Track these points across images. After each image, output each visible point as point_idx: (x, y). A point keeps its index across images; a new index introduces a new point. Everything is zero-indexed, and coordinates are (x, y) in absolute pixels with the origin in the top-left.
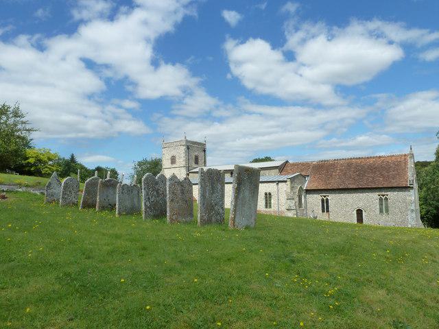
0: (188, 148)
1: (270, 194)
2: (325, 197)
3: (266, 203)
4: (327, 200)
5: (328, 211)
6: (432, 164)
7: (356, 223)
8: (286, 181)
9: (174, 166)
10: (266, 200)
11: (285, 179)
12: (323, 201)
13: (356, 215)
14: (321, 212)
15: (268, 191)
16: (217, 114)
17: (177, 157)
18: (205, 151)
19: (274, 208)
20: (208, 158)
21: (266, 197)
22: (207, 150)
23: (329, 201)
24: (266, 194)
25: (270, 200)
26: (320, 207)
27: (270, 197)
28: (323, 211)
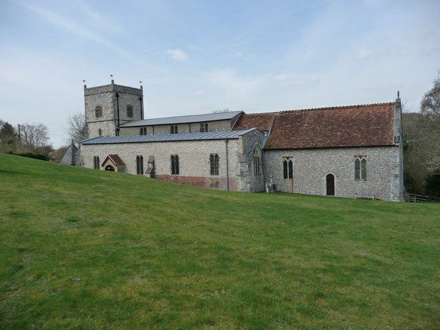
0: (117, 96)
3: (138, 167)
4: (291, 163)
5: (291, 177)
9: (100, 119)
12: (285, 163)
13: (325, 182)
14: (282, 177)
18: (141, 99)
28: (285, 177)
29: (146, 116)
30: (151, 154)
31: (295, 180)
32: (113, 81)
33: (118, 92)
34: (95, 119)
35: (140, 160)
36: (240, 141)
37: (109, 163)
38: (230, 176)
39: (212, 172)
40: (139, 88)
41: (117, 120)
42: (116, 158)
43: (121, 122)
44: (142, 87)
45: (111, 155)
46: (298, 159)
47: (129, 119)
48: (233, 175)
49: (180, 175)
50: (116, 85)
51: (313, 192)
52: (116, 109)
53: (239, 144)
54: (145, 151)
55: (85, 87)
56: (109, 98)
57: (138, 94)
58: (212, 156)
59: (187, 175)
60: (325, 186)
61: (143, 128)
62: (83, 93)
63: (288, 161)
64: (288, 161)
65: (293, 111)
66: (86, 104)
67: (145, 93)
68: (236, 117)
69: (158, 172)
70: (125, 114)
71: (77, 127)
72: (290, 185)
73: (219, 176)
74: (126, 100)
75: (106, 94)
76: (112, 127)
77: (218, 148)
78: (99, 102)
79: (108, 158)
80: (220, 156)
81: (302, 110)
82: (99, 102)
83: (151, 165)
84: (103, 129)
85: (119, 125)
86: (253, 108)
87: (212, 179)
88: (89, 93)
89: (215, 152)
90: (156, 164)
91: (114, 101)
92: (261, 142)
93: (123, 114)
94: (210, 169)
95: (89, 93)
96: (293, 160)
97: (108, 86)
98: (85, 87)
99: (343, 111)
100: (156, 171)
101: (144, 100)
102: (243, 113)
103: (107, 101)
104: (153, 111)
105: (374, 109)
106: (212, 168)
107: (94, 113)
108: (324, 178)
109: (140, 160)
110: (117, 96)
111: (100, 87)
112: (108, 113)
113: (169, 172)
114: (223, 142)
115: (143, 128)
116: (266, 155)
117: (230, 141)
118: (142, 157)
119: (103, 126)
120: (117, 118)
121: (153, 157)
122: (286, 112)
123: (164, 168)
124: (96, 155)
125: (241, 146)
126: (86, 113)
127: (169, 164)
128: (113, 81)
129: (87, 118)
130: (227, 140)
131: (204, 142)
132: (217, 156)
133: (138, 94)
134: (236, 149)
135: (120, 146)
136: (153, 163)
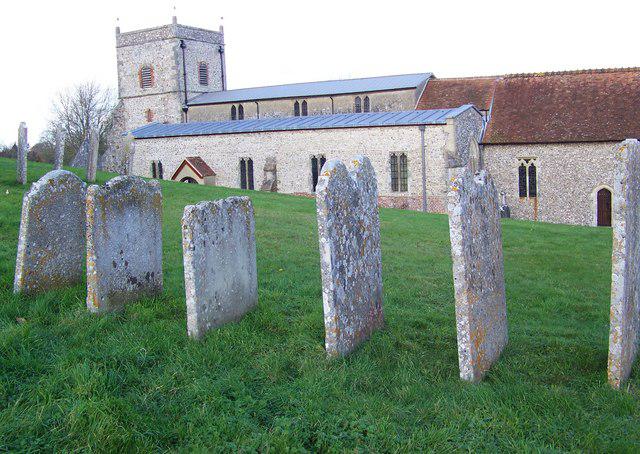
0: (183, 46)
4: (533, 169)
5: (533, 194)
9: (150, 90)
12: (522, 170)
14: (517, 195)
18: (221, 52)
26: (516, 185)
28: (522, 194)
29: (230, 86)
30: (271, 154)
31: (540, 199)
32: (175, 19)
33: (185, 38)
34: (139, 91)
35: (246, 167)
36: (449, 128)
37: (187, 172)
38: (429, 193)
39: (394, 187)
40: (218, 30)
41: (182, 91)
42: (199, 164)
44: (222, 28)
45: (191, 159)
46: (544, 158)
47: (204, 89)
48: (434, 190)
50: (179, 26)
52: (182, 72)
54: (256, 148)
55: (118, 30)
56: (170, 47)
57: (216, 41)
58: (393, 157)
61: (237, 106)
62: (113, 42)
63: (527, 166)
64: (527, 166)
65: (529, 75)
66: (120, 63)
67: (226, 40)
68: (421, 85)
69: (285, 188)
70: (196, 80)
71: (63, 110)
73: (409, 193)
74: (200, 51)
75: (161, 43)
76: (175, 105)
77: (406, 140)
78: (146, 56)
79: (185, 163)
80: (409, 156)
81: (547, 74)
82: (146, 56)
83: (270, 176)
84: (154, 109)
85: (186, 101)
86: (451, 68)
87: (395, 200)
88: (127, 41)
89: (399, 149)
91: (176, 55)
92: (476, 131)
93: (194, 79)
94: (390, 180)
95: (127, 41)
96: (537, 164)
97: (166, 27)
98: (118, 30)
99: (623, 76)
100: (279, 186)
101: (226, 52)
102: (432, 77)
103: (163, 57)
104: (243, 74)
105: (456, 89)
106: (394, 179)
107: (137, 79)
108: (594, 195)
109: (246, 167)
111: (147, 31)
112: (166, 78)
113: (235, 183)
114: (416, 130)
115: (300, 102)
116: (487, 150)
117: (428, 128)
118: (251, 162)
120: (183, 88)
121: (274, 160)
122: (517, 76)
123: (229, 177)
124: (156, 158)
125: (452, 137)
126: (120, 79)
127: (237, 174)
128: (175, 19)
129: (121, 90)
130: (422, 126)
131: (377, 131)
132: (403, 156)
133: (216, 41)
136: (274, 171)
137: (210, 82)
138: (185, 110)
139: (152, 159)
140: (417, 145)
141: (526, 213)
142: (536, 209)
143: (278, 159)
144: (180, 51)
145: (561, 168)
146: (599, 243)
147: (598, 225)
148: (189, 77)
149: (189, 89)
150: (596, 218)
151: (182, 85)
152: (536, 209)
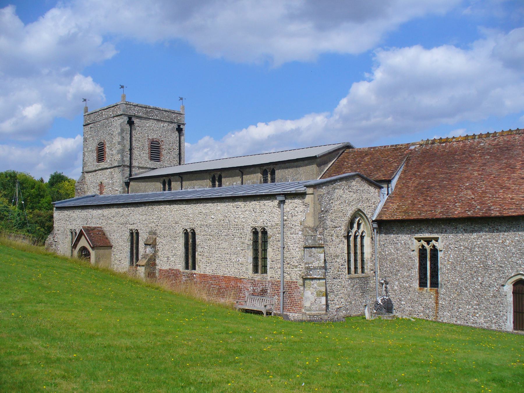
0: (131, 123)
1: (264, 232)
2: (428, 241)
3: (255, 259)
4: (435, 251)
5: (435, 284)
6: (354, 149)
7: (509, 325)
8: (302, 195)
9: (103, 165)
10: (256, 250)
11: (302, 189)
12: (422, 252)
13: (510, 299)
14: (416, 284)
15: (259, 224)
16: (385, 47)
17: (107, 145)
18: (180, 130)
19: (105, 194)
20: (186, 145)
21: (255, 242)
22: (185, 128)
23: (440, 255)
24: (255, 232)
25: (265, 250)
26: (416, 272)
27: (265, 242)
28: (423, 284)
31: (442, 291)
32: (124, 97)
35: (134, 236)
43: (135, 171)
47: (151, 164)
49: (197, 271)
51: (482, 320)
52: (128, 146)
53: (306, 205)
55: (86, 110)
59: (209, 271)
60: (511, 309)
64: (428, 248)
69: (162, 264)
72: (431, 302)
80: (270, 232)
84: (105, 181)
85: (131, 175)
87: (254, 283)
90: (159, 247)
91: (122, 131)
96: (439, 245)
100: (157, 261)
107: (95, 155)
110: (131, 123)
113: (180, 266)
119: (103, 177)
125: (310, 210)
128: (124, 97)
134: (301, 217)
135: (106, 212)
137: (162, 158)
138: (127, 184)
139: (70, 227)
140: (277, 219)
141: (427, 307)
142: (437, 303)
143: (158, 232)
144: (128, 127)
145: (467, 252)
146: (397, 354)
147: (516, 327)
148: (136, 152)
149: (135, 164)
150: (510, 317)
151: (127, 159)
152: (437, 303)
